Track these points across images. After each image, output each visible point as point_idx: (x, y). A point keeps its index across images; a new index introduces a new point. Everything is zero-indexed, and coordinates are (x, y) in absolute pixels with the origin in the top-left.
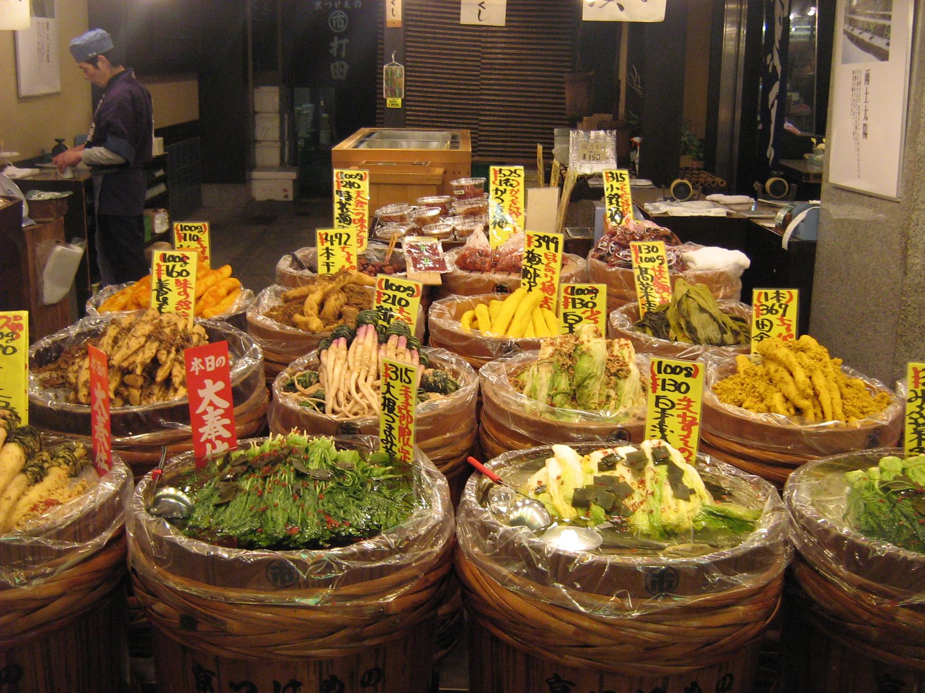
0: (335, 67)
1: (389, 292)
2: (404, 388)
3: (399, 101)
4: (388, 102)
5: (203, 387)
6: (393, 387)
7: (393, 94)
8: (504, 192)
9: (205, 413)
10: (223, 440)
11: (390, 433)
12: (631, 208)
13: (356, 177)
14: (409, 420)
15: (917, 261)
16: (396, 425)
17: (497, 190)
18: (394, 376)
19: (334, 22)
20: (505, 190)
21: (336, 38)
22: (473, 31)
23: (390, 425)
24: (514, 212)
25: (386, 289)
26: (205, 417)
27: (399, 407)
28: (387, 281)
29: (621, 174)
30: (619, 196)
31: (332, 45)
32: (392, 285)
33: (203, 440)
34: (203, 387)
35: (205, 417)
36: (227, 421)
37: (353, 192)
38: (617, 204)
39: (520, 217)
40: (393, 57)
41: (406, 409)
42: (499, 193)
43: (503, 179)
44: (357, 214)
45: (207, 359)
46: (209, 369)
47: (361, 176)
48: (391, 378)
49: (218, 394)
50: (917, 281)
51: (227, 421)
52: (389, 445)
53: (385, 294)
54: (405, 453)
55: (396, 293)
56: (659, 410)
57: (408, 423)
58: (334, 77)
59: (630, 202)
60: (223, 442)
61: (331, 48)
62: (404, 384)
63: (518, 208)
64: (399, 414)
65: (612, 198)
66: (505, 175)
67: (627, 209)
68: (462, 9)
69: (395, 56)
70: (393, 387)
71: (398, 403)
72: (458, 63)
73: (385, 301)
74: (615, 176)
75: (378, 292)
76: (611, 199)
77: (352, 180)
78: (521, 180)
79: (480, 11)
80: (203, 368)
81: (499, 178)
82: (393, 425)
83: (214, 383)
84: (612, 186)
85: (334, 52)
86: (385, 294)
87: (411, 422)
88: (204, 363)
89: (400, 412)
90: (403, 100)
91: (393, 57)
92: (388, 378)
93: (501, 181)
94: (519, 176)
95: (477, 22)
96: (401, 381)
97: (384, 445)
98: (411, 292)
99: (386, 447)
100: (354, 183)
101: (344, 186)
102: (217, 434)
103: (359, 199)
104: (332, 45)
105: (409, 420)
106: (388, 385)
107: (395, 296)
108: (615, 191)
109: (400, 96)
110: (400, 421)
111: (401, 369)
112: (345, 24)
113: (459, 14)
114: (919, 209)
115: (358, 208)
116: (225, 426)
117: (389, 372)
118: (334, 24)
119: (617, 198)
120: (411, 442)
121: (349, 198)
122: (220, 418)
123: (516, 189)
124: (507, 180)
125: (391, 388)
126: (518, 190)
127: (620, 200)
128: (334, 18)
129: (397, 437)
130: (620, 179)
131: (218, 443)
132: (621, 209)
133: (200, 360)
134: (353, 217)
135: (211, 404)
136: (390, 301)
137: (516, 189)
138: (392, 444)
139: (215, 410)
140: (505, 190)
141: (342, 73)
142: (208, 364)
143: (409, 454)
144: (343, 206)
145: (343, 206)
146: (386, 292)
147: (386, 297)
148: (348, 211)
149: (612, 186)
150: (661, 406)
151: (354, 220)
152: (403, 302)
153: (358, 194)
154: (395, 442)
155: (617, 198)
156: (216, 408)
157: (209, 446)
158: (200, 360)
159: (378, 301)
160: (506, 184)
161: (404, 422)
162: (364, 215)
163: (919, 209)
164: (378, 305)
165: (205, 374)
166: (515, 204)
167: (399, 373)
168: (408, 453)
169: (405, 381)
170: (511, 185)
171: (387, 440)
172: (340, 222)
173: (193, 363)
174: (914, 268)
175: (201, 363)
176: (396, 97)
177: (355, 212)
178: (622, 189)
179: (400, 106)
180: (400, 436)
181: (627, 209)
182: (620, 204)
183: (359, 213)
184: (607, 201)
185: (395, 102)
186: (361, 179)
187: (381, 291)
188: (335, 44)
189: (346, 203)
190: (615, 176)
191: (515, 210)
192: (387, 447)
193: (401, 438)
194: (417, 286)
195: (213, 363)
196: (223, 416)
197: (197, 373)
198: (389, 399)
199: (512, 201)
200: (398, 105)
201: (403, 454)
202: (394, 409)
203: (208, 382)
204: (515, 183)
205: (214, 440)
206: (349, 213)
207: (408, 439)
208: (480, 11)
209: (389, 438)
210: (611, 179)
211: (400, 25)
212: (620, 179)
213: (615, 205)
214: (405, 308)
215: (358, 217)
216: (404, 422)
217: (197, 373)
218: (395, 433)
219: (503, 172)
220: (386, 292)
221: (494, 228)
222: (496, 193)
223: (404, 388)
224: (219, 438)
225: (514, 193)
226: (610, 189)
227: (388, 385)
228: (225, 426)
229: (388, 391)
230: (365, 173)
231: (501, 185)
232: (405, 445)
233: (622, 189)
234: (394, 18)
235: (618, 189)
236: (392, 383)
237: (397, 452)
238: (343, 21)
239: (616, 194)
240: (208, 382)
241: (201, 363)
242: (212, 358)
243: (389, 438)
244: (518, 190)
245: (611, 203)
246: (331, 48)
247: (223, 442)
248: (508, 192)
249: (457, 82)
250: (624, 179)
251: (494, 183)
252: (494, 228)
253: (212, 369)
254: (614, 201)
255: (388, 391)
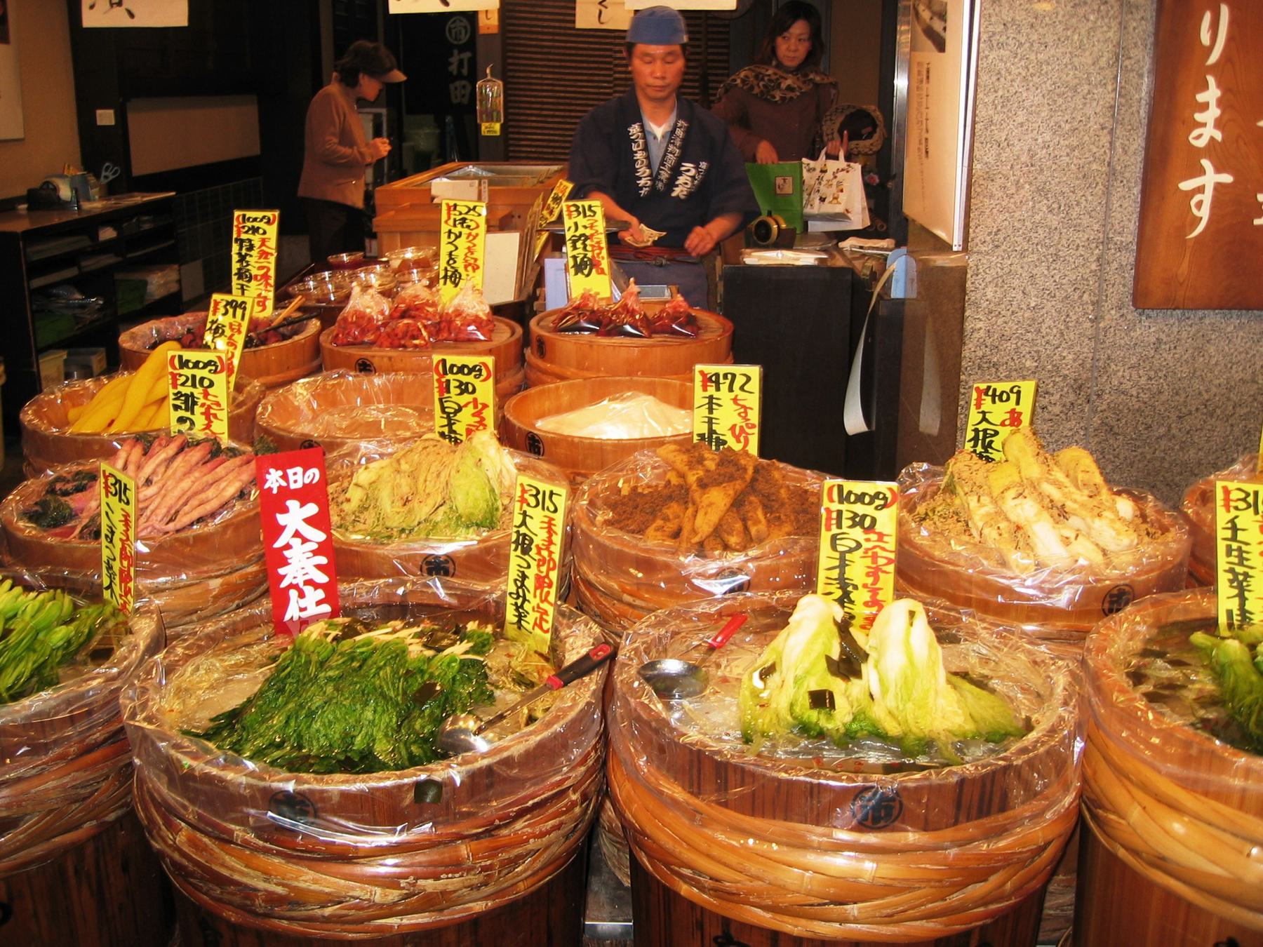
0: (456, 88)
1: (186, 372)
2: (546, 520)
3: (497, 127)
4: (483, 128)
5: (285, 510)
6: (531, 517)
7: (490, 119)
8: (458, 236)
9: (288, 547)
10: (316, 586)
11: (523, 584)
12: (604, 253)
13: (261, 220)
14: (551, 565)
15: (980, 325)
16: (531, 573)
17: (450, 232)
18: (532, 501)
19: (453, 31)
20: (460, 233)
21: (456, 52)
22: (593, 36)
23: (523, 573)
24: (470, 264)
25: (181, 368)
26: (287, 553)
27: (537, 546)
28: (180, 357)
29: (590, 207)
30: (587, 238)
31: (451, 60)
32: (188, 361)
33: (284, 584)
34: (285, 510)
35: (287, 553)
36: (323, 560)
37: (256, 239)
38: (585, 248)
39: (477, 271)
40: (488, 71)
41: (547, 548)
42: (453, 237)
43: (458, 218)
44: (260, 268)
45: (290, 472)
46: (293, 486)
47: (269, 219)
48: (528, 505)
49: (309, 521)
50: (980, 354)
51: (323, 560)
52: (519, 602)
53: (181, 375)
54: (542, 614)
55: (195, 371)
56: (837, 555)
57: (549, 569)
58: (455, 101)
59: (604, 245)
60: (316, 589)
61: (451, 64)
62: (546, 513)
63: (476, 260)
64: (537, 557)
65: (577, 241)
66: (461, 214)
67: (599, 254)
68: (577, 9)
69: (491, 71)
70: (531, 517)
71: (537, 541)
72: (585, 78)
73: (183, 384)
74: (581, 210)
75: (172, 373)
76: (574, 243)
77: (256, 224)
78: (482, 221)
79: (600, 13)
80: (284, 484)
81: (452, 217)
82: (527, 572)
83: (302, 505)
84: (576, 224)
85: (453, 68)
86: (181, 375)
87: (553, 569)
88: (285, 477)
89: (539, 553)
90: (502, 127)
91: (488, 71)
92: (525, 505)
93: (455, 220)
94: (480, 215)
95: (597, 26)
96: (543, 508)
97: (513, 601)
98: (213, 368)
99: (516, 604)
100: (258, 228)
101: (246, 232)
102: (307, 577)
103: (264, 248)
104: (451, 60)
105: (551, 565)
106: (525, 514)
107: (194, 377)
108: (581, 231)
109: (498, 121)
110: (539, 566)
111: (544, 493)
112: (466, 32)
113: (574, 15)
114: (979, 253)
115: (262, 260)
116: (319, 567)
117: (526, 496)
118: (453, 35)
119: (585, 241)
120: (552, 598)
121: (251, 248)
122: (311, 554)
123: (474, 233)
124: (464, 220)
125: (528, 519)
126: (477, 235)
127: (588, 242)
128: (453, 26)
129: (532, 589)
130: (588, 213)
131: (308, 590)
132: (589, 255)
133: (280, 473)
134: (254, 272)
135: (297, 534)
136: (189, 383)
137: (474, 233)
138: (525, 600)
139: (303, 543)
140: (460, 233)
141: (463, 96)
142: (292, 478)
143: (547, 615)
144: (242, 258)
145: (242, 258)
146: (181, 372)
147: (183, 379)
148: (248, 265)
149: (576, 224)
150: (840, 548)
151: (256, 276)
152: (206, 383)
153: (263, 242)
154: (529, 596)
155: (585, 241)
156: (305, 540)
157: (293, 594)
158: (280, 473)
159: (175, 386)
160: (462, 224)
161: (544, 569)
162: (269, 269)
163: (979, 253)
164: (176, 391)
165: (286, 493)
166: (472, 253)
167: (540, 497)
168: (546, 612)
169: (548, 509)
170: (468, 227)
171: (518, 593)
172: (238, 279)
173: (268, 477)
174: (976, 335)
175: (281, 477)
176: (492, 121)
177: (257, 265)
178: (592, 226)
179: (498, 134)
180: (536, 588)
181: (599, 254)
182: (589, 248)
183: (262, 268)
184: (569, 244)
185: (492, 128)
186: (269, 222)
187: (176, 372)
188: (455, 59)
189: (246, 255)
190: (581, 210)
191: (472, 261)
192: (516, 604)
193: (538, 592)
194: (220, 358)
195: (299, 477)
196: (316, 553)
197: (275, 491)
198: (525, 535)
199: (469, 248)
200: (495, 132)
201: (538, 615)
202: (531, 549)
203: (293, 504)
204: (473, 225)
205: (301, 585)
206: (249, 267)
207: (548, 593)
208: (600, 13)
209: (520, 591)
210: (575, 214)
211: (495, 31)
212: (588, 213)
213: (580, 251)
214: (210, 390)
215: (262, 272)
216: (544, 569)
217: (275, 491)
218: (530, 583)
219: (458, 208)
220: (181, 372)
221: (445, 283)
222: (449, 237)
223: (546, 520)
224: (309, 582)
225: (471, 238)
226: (573, 228)
227: (525, 514)
228: (319, 567)
229: (524, 523)
230: (274, 216)
231: (455, 225)
232: (542, 601)
233: (592, 226)
234: (488, 22)
235: (585, 227)
236: (530, 511)
237: (530, 611)
238: (463, 31)
239: (583, 235)
240: (293, 504)
241: (281, 477)
242: (299, 470)
243: (520, 591)
244: (477, 235)
245: (575, 248)
246: (451, 64)
247: (316, 589)
248: (464, 236)
249: (584, 102)
250: (595, 213)
251: (446, 222)
252: (445, 283)
253: (299, 485)
254: (579, 244)
255: (524, 523)
